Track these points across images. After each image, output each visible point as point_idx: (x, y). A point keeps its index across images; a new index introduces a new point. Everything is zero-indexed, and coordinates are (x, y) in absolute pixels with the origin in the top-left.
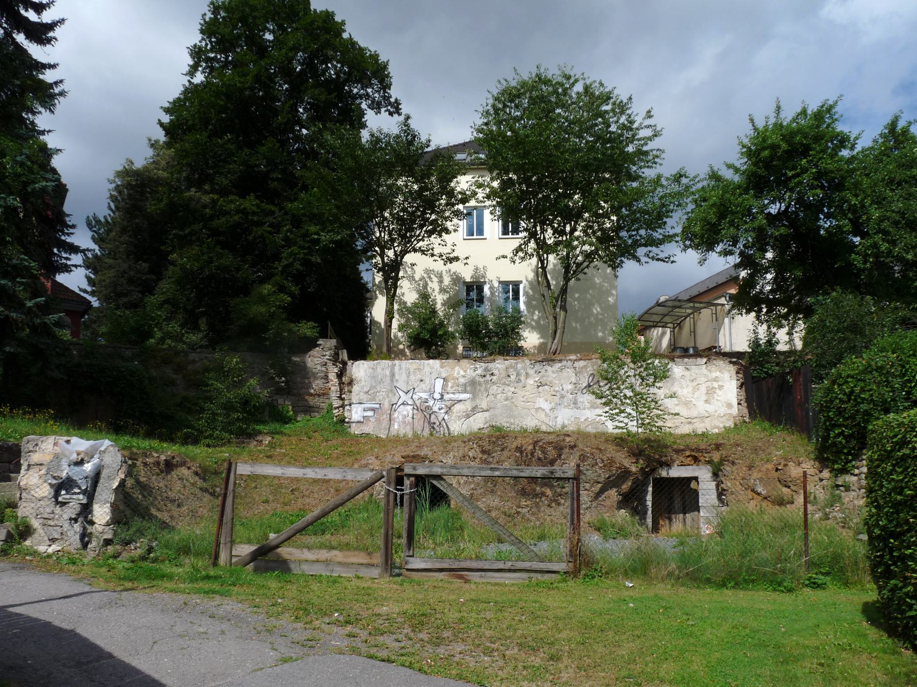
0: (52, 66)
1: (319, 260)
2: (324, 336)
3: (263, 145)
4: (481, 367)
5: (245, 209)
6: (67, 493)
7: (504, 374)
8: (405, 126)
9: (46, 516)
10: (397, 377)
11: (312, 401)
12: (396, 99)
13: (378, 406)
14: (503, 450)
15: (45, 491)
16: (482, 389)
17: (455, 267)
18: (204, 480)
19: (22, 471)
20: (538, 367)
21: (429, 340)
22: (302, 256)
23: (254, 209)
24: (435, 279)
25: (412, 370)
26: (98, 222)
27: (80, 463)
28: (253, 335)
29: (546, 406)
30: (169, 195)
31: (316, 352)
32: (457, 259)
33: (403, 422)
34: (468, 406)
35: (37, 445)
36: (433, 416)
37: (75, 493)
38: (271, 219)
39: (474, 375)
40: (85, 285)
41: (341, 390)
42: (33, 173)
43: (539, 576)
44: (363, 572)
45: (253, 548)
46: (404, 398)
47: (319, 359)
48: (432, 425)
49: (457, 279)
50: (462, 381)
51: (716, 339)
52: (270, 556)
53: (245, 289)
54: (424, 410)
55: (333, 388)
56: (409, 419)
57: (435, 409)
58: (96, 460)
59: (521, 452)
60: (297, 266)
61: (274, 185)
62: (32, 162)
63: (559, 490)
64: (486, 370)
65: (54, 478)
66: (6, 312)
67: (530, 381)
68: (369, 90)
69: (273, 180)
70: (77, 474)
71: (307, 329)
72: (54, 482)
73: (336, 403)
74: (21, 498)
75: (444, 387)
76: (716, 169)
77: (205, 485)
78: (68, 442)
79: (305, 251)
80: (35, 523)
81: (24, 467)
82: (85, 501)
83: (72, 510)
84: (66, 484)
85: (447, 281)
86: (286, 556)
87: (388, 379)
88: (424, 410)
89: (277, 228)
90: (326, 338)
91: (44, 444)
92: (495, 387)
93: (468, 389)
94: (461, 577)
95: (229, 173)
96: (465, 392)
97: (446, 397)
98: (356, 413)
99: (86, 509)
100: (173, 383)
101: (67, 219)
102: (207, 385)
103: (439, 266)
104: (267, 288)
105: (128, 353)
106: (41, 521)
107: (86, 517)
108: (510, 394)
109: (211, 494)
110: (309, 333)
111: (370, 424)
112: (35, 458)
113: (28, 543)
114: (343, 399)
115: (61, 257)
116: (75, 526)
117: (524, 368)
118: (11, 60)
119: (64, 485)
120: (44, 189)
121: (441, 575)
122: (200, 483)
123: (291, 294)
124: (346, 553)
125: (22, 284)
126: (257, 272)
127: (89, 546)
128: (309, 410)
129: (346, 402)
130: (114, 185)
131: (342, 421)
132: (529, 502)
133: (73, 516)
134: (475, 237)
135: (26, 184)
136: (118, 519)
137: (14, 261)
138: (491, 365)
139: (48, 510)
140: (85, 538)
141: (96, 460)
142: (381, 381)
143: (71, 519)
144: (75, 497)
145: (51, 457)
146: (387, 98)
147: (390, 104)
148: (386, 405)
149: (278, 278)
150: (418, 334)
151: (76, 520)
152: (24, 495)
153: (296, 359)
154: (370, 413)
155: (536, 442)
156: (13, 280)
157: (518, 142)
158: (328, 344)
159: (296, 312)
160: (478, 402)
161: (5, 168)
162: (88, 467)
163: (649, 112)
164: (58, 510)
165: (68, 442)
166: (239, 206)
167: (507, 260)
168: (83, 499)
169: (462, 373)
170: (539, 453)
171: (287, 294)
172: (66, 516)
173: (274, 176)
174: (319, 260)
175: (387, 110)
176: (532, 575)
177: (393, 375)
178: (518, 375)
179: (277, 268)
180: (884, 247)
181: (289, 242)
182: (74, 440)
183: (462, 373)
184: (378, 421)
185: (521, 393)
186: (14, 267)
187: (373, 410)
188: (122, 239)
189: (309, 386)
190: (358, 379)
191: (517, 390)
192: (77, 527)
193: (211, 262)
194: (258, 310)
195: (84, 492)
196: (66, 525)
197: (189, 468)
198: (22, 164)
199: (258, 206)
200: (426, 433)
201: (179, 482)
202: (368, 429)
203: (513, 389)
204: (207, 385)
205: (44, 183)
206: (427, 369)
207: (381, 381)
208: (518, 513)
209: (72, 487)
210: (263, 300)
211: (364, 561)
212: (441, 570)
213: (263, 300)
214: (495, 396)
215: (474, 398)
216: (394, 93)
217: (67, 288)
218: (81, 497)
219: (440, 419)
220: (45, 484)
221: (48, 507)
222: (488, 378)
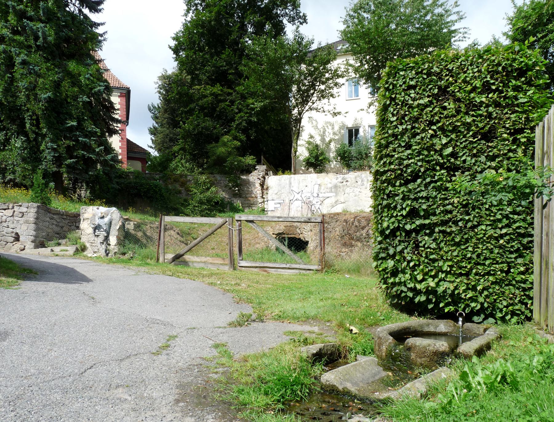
0: (103, 24)
1: (256, 120)
2: (259, 162)
3: (223, 53)
5: (214, 93)
7: (354, 181)
8: (297, 32)
10: (293, 184)
12: (304, 14)
13: (282, 201)
14: (336, 222)
15: (91, 230)
16: (341, 190)
17: (339, 118)
18: (182, 237)
19: (81, 222)
21: (317, 163)
22: (246, 118)
23: (220, 92)
24: (330, 127)
25: (301, 180)
26: (154, 107)
27: (103, 217)
28: (219, 166)
30: (177, 88)
31: (254, 173)
32: (339, 113)
34: (333, 200)
36: (313, 207)
38: (230, 98)
39: (336, 181)
40: (150, 144)
41: (263, 193)
42: (94, 83)
43: (304, 271)
44: (222, 268)
45: (173, 255)
47: (254, 177)
50: (330, 186)
52: (181, 259)
53: (217, 139)
55: (258, 192)
58: (109, 217)
59: (347, 223)
60: (244, 124)
61: (230, 77)
62: (93, 77)
63: (365, 243)
66: (88, 155)
68: (287, 11)
69: (230, 74)
71: (249, 160)
73: (260, 200)
76: (497, 37)
77: (182, 239)
78: (98, 209)
79: (248, 115)
80: (88, 245)
81: (82, 220)
82: (106, 235)
83: (101, 238)
86: (188, 260)
87: (288, 186)
89: (232, 102)
90: (261, 164)
92: (348, 189)
93: (333, 190)
94: (266, 271)
95: (206, 72)
96: (331, 192)
97: (320, 195)
98: (270, 206)
99: (107, 238)
100: (180, 192)
101: (115, 106)
102: (191, 191)
103: (330, 118)
104: (226, 138)
105: (157, 177)
107: (107, 242)
108: (357, 193)
109: (185, 244)
110: (251, 162)
111: (278, 211)
112: (86, 216)
113: (85, 253)
114: (264, 198)
115: (114, 126)
117: (366, 177)
118: (81, 24)
119: (97, 228)
120: (99, 91)
121: (256, 270)
122: (179, 238)
123: (240, 141)
124: (213, 258)
125: (94, 140)
126: (224, 129)
129: (265, 200)
130: (158, 85)
132: (347, 250)
134: (354, 98)
135: (91, 89)
136: (120, 243)
137: (89, 129)
141: (109, 217)
142: (284, 187)
143: (101, 243)
145: (91, 215)
146: (298, 14)
147: (300, 17)
148: (287, 201)
149: (233, 132)
150: (308, 160)
153: (244, 177)
154: (279, 205)
155: (356, 217)
156: (90, 139)
157: (365, 35)
158: (261, 168)
159: (242, 151)
160: (339, 198)
161: (81, 82)
162: (106, 220)
163: (456, 2)
165: (98, 209)
166: (211, 91)
167: (365, 112)
169: (329, 181)
170: (356, 223)
171: (238, 140)
172: (99, 242)
173: (230, 71)
174: (256, 120)
175: (299, 21)
176: (301, 271)
177: (290, 183)
178: (362, 181)
179: (232, 126)
181: (240, 111)
182: (101, 208)
183: (329, 181)
184: (283, 210)
186: (90, 132)
188: (164, 116)
190: (271, 186)
191: (361, 190)
192: (104, 246)
193: (199, 125)
194: (221, 150)
195: (105, 231)
196: (99, 246)
197: (174, 231)
198: (88, 79)
199: (222, 90)
201: (169, 237)
203: (359, 190)
204: (191, 191)
205: (99, 88)
207: (284, 187)
208: (340, 255)
210: (225, 144)
211: (222, 263)
212: (256, 267)
213: (225, 144)
214: (349, 194)
215: (336, 196)
216: (303, 10)
217: (138, 146)
218: (104, 233)
219: (317, 208)
222: (345, 183)
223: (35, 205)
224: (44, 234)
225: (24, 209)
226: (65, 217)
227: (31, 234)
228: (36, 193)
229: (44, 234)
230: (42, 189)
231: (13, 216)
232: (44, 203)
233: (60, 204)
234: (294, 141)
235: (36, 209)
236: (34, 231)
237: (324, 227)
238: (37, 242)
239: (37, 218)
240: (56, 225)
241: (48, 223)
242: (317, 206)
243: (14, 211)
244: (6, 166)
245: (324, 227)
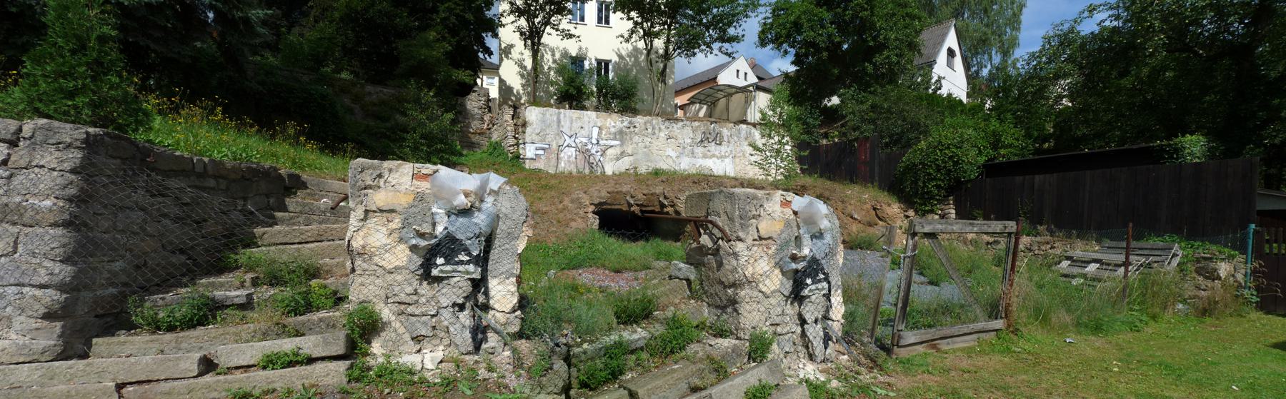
4: (627, 120)
6: (447, 262)
9: (403, 297)
11: (475, 139)
20: (667, 123)
29: (673, 154)
33: (568, 161)
34: (617, 151)
35: (380, 176)
37: (461, 262)
46: (568, 141)
48: (591, 165)
49: (565, 54)
50: (613, 130)
51: (745, 113)
54: (584, 152)
56: (573, 159)
57: (593, 151)
64: (630, 123)
65: (422, 235)
67: (662, 134)
70: (463, 229)
72: (423, 243)
73: (512, 141)
74: (353, 270)
75: (600, 134)
80: (386, 313)
82: (477, 276)
83: (456, 288)
84: (448, 247)
85: (558, 56)
88: (584, 152)
91: (394, 175)
96: (615, 139)
98: (529, 151)
106: (395, 307)
112: (379, 198)
116: (461, 315)
127: (484, 346)
128: (471, 146)
131: (518, 157)
133: (460, 301)
138: (634, 119)
139: (409, 290)
140: (479, 333)
143: (454, 305)
144: (461, 268)
145: (410, 199)
148: (554, 146)
151: (462, 307)
152: (358, 262)
154: (541, 152)
162: (480, 219)
164: (425, 289)
168: (474, 271)
177: (559, 121)
180: (894, 59)
184: (548, 158)
185: (656, 143)
187: (543, 149)
189: (469, 126)
192: (465, 317)
200: (587, 171)
202: (540, 165)
206: (586, 119)
207: (550, 126)
209: (457, 253)
218: (471, 267)
220: (403, 246)
221: (407, 285)
223: (70, 132)
224: (118, 265)
226: (212, 183)
229: (118, 265)
233: (195, 136)
236: (65, 260)
237: (1117, 265)
238: (82, 310)
239: (79, 200)
240: (177, 220)
241: (137, 216)
242: (598, 156)
245: (1117, 265)
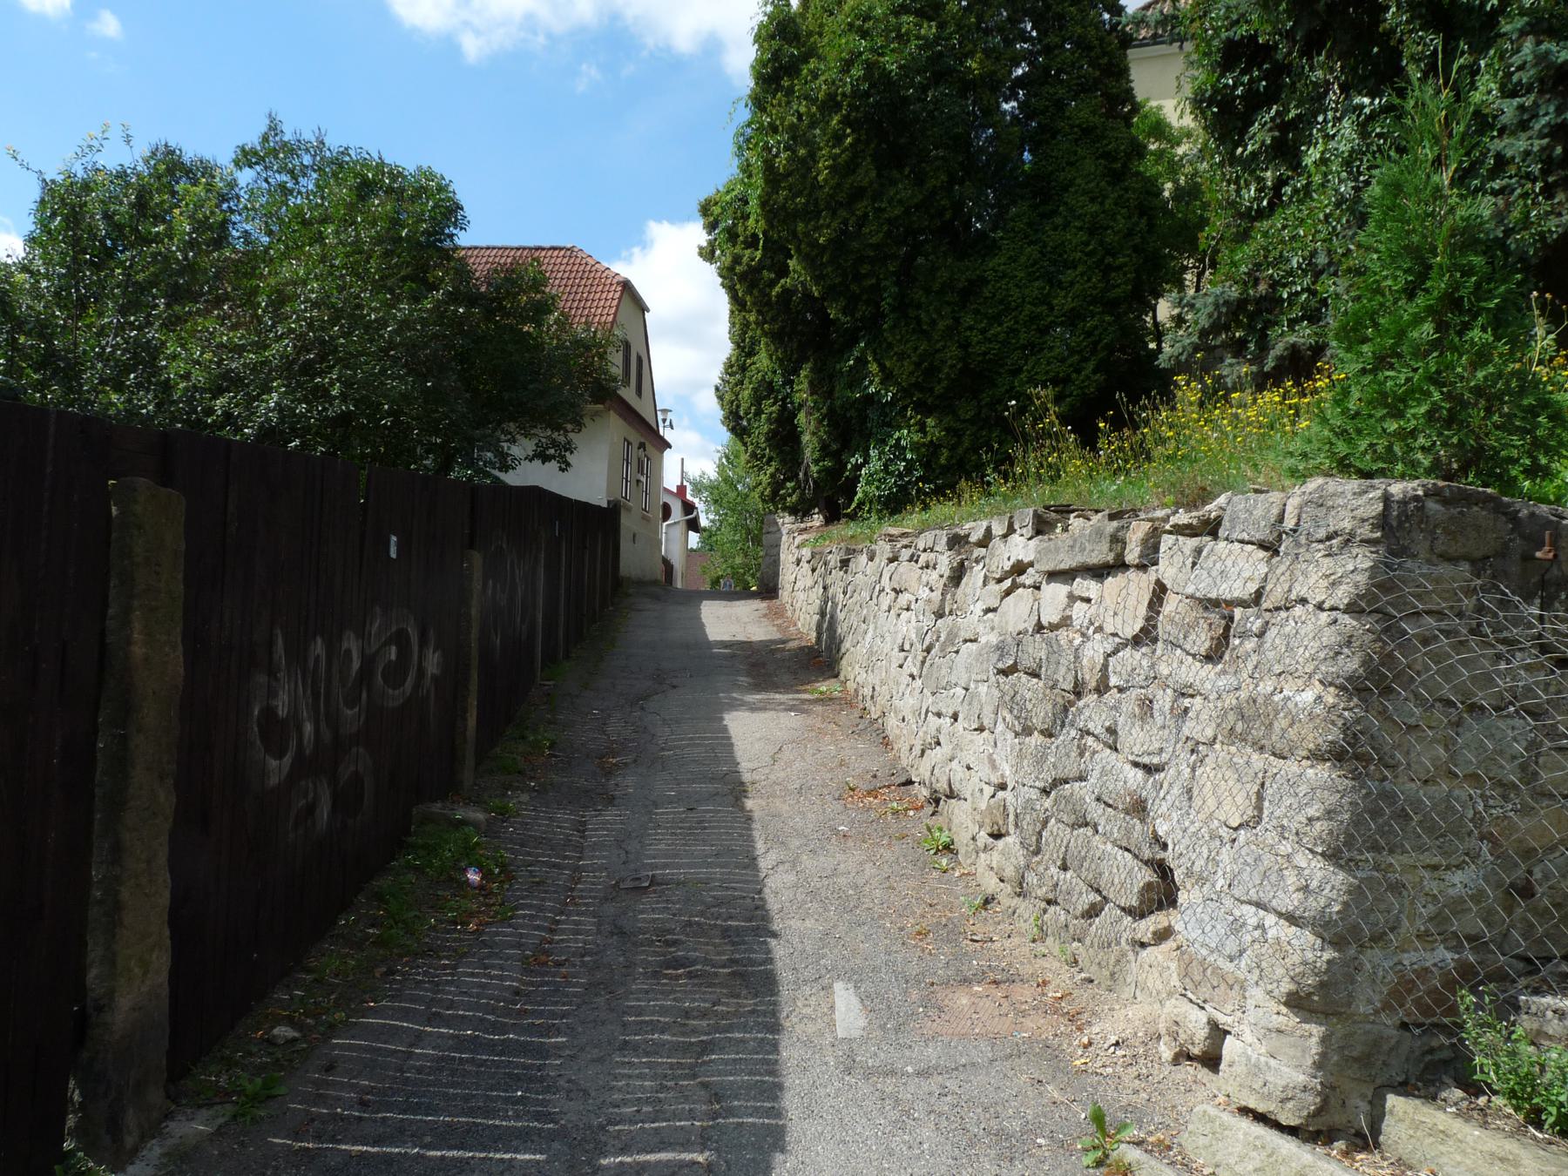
223: (1354, 502)
224: (1459, 881)
225: (1234, 569)
227: (1290, 900)
228: (1382, 361)
229: (1459, 881)
230: (1452, 301)
231: (1146, 637)
232: (1476, 459)
234: (95, 953)
235: (1361, 561)
236: (1332, 856)
239: (1370, 685)
243: (1160, 590)
244: (1275, 285)
